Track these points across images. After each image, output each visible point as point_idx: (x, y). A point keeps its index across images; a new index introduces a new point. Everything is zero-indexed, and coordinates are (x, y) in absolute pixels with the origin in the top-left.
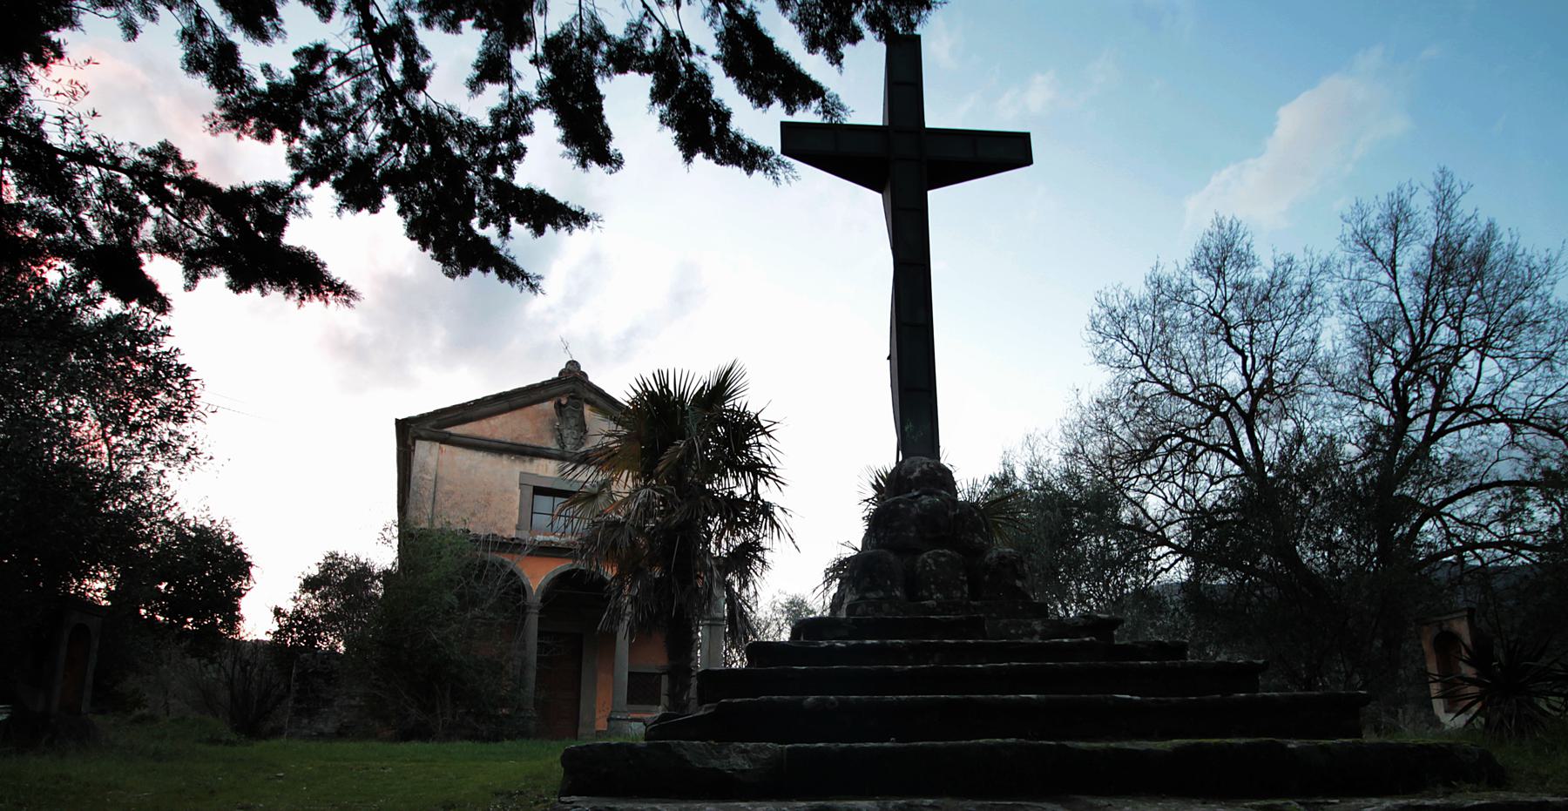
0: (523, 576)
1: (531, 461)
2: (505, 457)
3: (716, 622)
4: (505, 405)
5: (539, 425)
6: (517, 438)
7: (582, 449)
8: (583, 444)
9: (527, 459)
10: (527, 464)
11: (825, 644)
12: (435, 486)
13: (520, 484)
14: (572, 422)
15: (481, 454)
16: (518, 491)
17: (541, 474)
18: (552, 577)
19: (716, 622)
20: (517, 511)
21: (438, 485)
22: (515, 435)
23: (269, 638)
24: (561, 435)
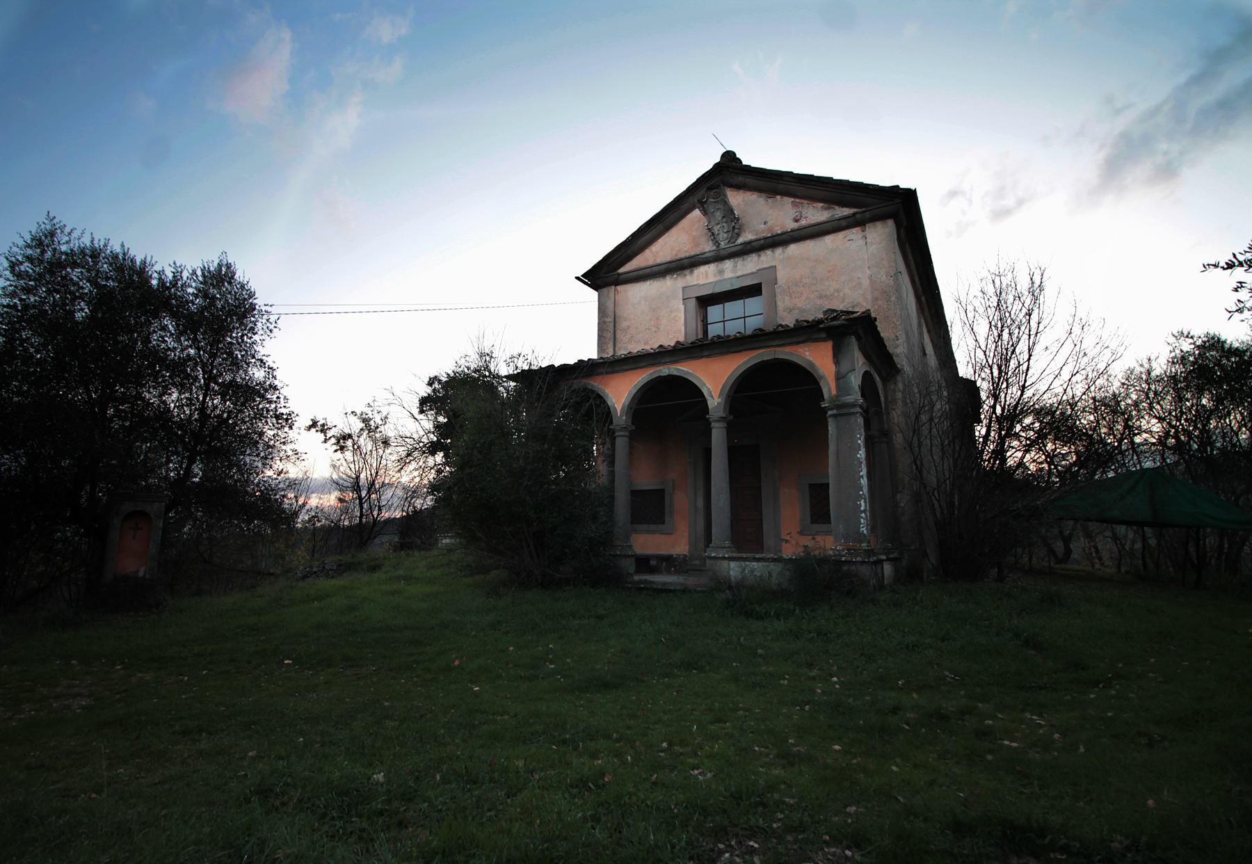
0: (607, 396)
1: (692, 272)
2: (668, 278)
3: (844, 411)
4: (660, 227)
5: (694, 233)
6: (676, 255)
7: (740, 240)
8: (738, 235)
9: (687, 272)
10: (688, 277)
11: (1014, 745)
12: (615, 326)
13: (684, 299)
14: (719, 215)
15: (648, 283)
16: (682, 307)
17: (701, 282)
18: (635, 391)
19: (844, 411)
20: (683, 328)
21: (617, 325)
22: (675, 252)
23: (960, 376)
24: (713, 234)
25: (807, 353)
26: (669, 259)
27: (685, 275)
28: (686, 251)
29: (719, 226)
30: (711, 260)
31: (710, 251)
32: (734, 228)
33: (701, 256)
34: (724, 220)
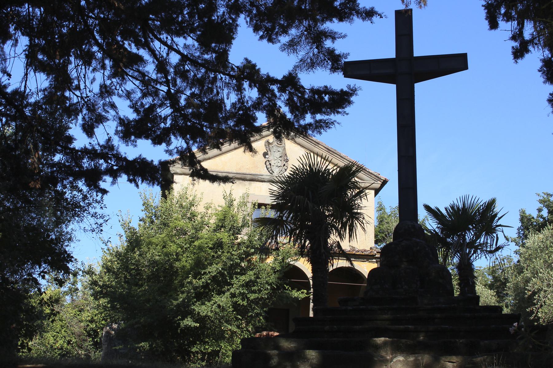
14: (278, 155)
25: (365, 267)
26: (235, 171)
27: (245, 185)
28: (248, 169)
29: (276, 161)
30: (266, 180)
31: (267, 175)
32: (284, 165)
33: (260, 176)
34: (280, 158)
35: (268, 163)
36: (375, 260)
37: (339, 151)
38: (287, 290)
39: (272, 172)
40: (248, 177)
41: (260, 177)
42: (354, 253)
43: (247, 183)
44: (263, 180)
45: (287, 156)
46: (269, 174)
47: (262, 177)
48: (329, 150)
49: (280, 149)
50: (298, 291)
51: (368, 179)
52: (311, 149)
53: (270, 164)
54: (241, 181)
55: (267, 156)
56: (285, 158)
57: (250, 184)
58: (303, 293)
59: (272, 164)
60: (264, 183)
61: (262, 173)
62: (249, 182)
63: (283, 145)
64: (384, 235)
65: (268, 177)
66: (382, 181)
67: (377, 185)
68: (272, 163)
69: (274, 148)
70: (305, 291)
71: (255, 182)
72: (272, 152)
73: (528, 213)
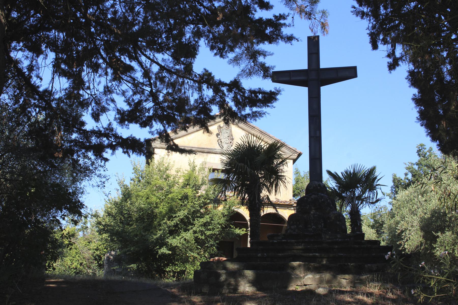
14: (226, 135)
32: (231, 142)
34: (228, 138)
35: (219, 141)
36: (293, 208)
37: (268, 133)
38: (232, 228)
39: (222, 147)
40: (206, 150)
41: (214, 151)
42: (278, 203)
43: (205, 154)
44: (216, 152)
45: (233, 136)
46: (220, 148)
47: (216, 150)
48: (261, 132)
49: (228, 131)
50: (239, 229)
51: (289, 152)
52: (249, 132)
53: (221, 142)
54: (201, 153)
55: (219, 136)
56: (232, 138)
57: (207, 155)
58: (243, 230)
59: (223, 141)
60: (216, 155)
61: (216, 148)
62: (206, 154)
63: (230, 128)
64: (299, 191)
65: (219, 151)
66: (298, 154)
67: (295, 156)
68: (223, 141)
69: (224, 130)
70: (245, 229)
71: (211, 154)
72: (223, 133)
73: (398, 176)
